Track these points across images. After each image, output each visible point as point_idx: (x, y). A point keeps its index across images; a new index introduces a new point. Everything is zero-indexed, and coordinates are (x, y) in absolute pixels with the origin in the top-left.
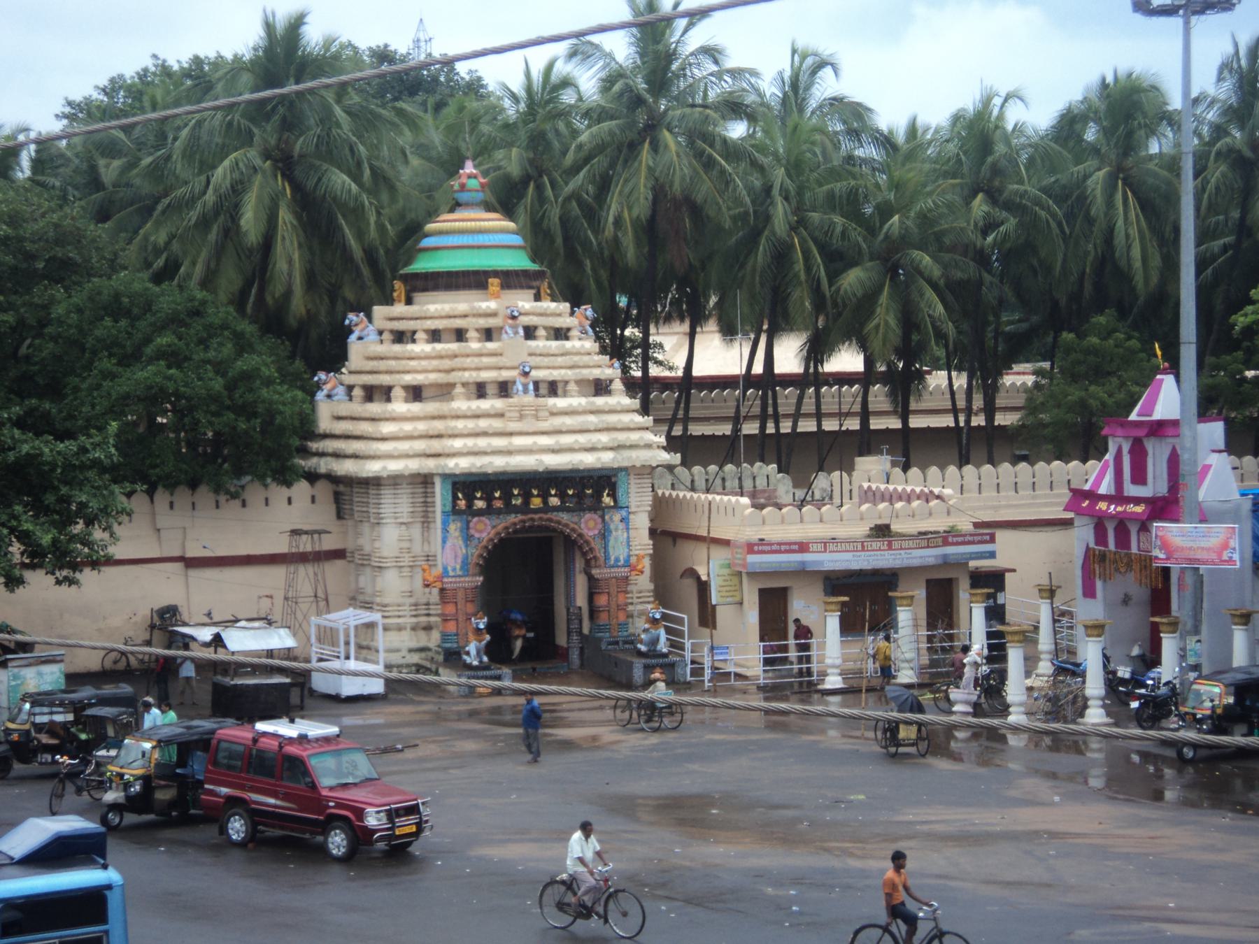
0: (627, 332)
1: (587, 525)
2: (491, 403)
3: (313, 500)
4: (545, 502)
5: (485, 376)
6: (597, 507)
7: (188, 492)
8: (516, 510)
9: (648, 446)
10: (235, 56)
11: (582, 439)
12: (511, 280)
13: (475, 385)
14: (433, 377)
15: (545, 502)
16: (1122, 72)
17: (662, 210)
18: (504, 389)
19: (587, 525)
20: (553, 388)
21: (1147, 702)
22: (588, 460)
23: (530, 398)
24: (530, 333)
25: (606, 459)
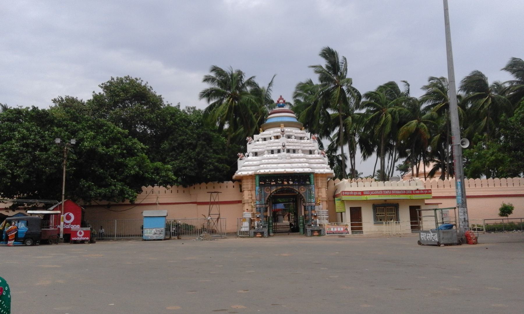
0: (429, 151)
1: (302, 190)
2: (276, 155)
3: (234, 187)
4: (288, 183)
5: (273, 148)
6: (305, 185)
7: (198, 184)
8: (280, 185)
9: (323, 168)
10: (105, 88)
11: (300, 165)
12: (288, 124)
13: (276, 151)
14: (260, 150)
15: (288, 183)
16: (149, 85)
17: (326, 107)
18: (279, 151)
19: (302, 190)
20: (294, 151)
21: (110, 132)
22: (300, 170)
23: (285, 153)
24: (289, 137)
25: (307, 170)
